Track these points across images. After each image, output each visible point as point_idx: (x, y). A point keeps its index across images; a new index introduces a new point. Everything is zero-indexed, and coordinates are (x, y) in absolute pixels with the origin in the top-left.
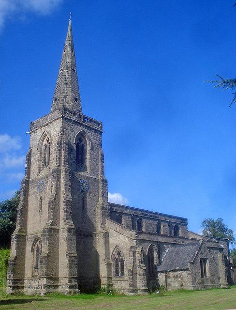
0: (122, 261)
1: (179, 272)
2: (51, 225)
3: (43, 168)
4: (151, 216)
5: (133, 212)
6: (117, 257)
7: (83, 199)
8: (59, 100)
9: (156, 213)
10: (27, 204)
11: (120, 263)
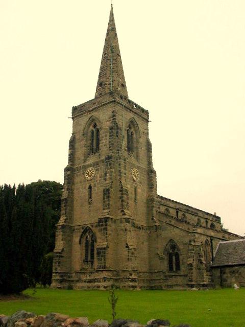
0: (177, 256)
1: (236, 268)
2: (108, 214)
3: (89, 155)
4: (192, 212)
5: (185, 208)
6: (171, 251)
7: (135, 189)
8: (105, 84)
9: (195, 209)
10: (72, 193)
11: (174, 258)
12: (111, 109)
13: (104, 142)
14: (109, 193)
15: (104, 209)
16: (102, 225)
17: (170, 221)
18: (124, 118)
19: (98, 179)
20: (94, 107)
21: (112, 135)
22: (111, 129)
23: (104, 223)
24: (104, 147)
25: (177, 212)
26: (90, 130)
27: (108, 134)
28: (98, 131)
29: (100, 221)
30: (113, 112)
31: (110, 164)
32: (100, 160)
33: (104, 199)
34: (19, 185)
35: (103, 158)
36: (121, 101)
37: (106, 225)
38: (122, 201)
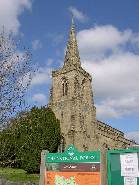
12: (75, 73)
13: (71, 90)
14: (74, 117)
15: (71, 126)
16: (71, 135)
17: (104, 134)
18: (81, 78)
19: (67, 109)
20: (65, 72)
21: (76, 87)
22: (75, 83)
23: (72, 133)
24: (71, 93)
25: (105, 129)
26: (62, 83)
27: (73, 86)
28: (67, 84)
29: (69, 132)
30: (76, 75)
31: (75, 102)
32: (68, 99)
33: (71, 120)
34: (42, 107)
35: (70, 98)
36: (80, 69)
37: (73, 134)
38: (81, 122)
